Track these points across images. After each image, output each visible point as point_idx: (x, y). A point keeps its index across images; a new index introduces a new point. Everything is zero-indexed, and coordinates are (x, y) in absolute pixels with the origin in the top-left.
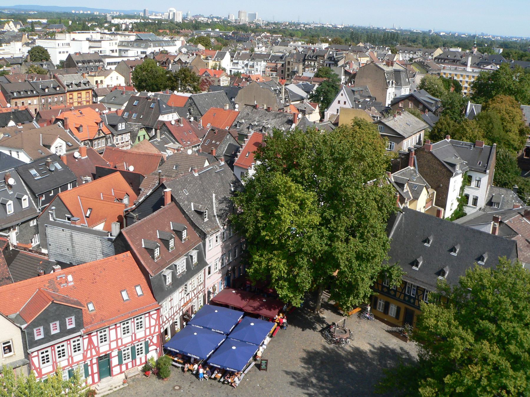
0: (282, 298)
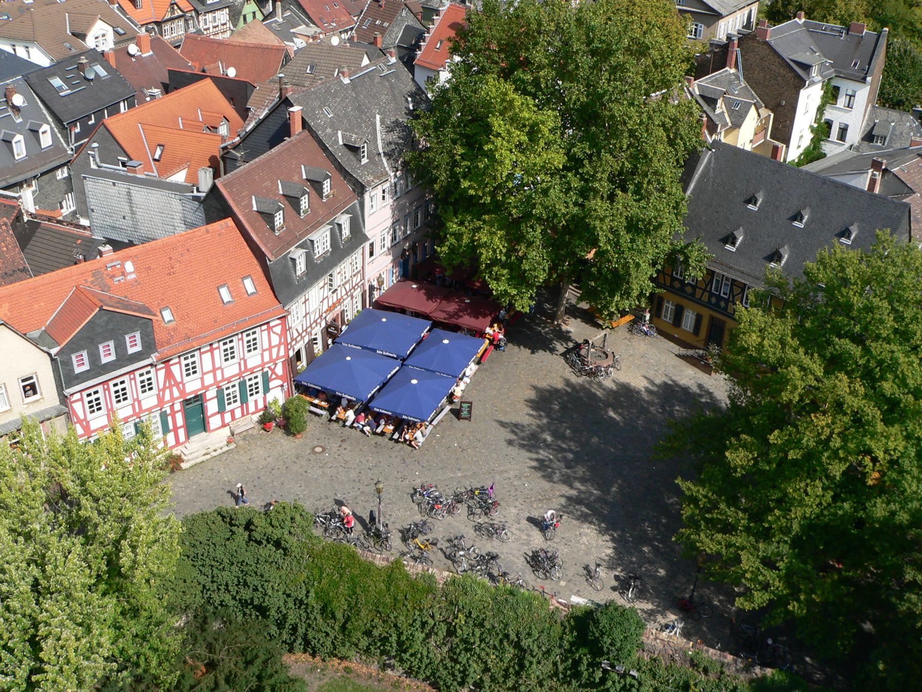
0: (498, 298)
